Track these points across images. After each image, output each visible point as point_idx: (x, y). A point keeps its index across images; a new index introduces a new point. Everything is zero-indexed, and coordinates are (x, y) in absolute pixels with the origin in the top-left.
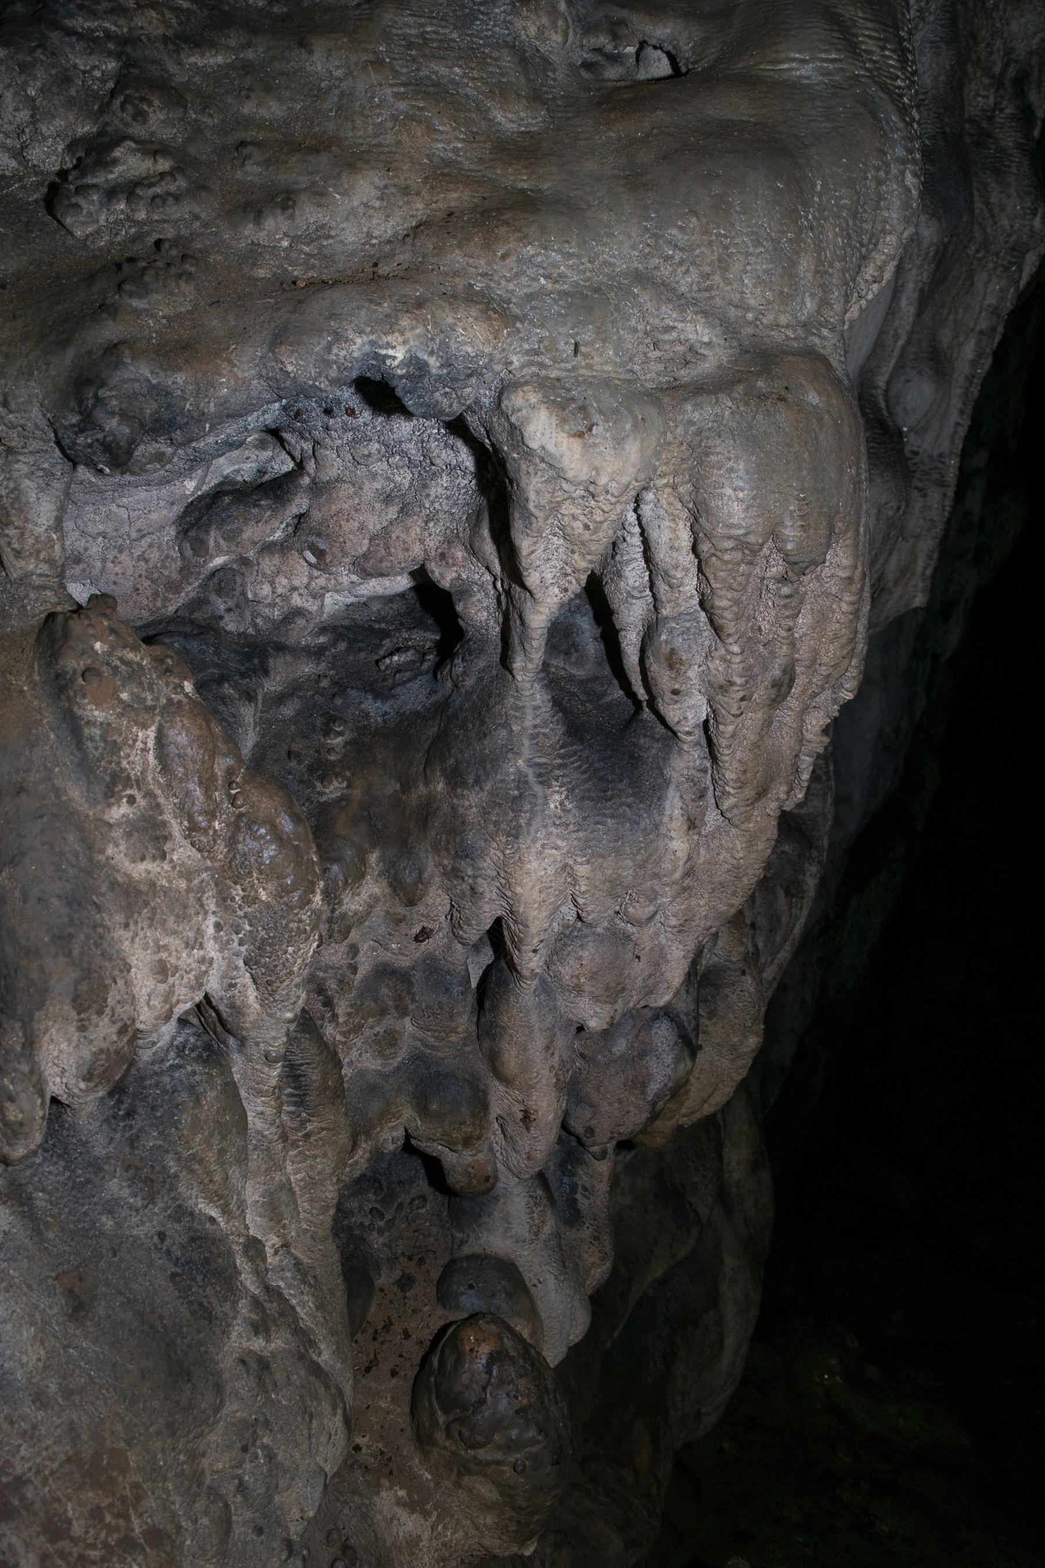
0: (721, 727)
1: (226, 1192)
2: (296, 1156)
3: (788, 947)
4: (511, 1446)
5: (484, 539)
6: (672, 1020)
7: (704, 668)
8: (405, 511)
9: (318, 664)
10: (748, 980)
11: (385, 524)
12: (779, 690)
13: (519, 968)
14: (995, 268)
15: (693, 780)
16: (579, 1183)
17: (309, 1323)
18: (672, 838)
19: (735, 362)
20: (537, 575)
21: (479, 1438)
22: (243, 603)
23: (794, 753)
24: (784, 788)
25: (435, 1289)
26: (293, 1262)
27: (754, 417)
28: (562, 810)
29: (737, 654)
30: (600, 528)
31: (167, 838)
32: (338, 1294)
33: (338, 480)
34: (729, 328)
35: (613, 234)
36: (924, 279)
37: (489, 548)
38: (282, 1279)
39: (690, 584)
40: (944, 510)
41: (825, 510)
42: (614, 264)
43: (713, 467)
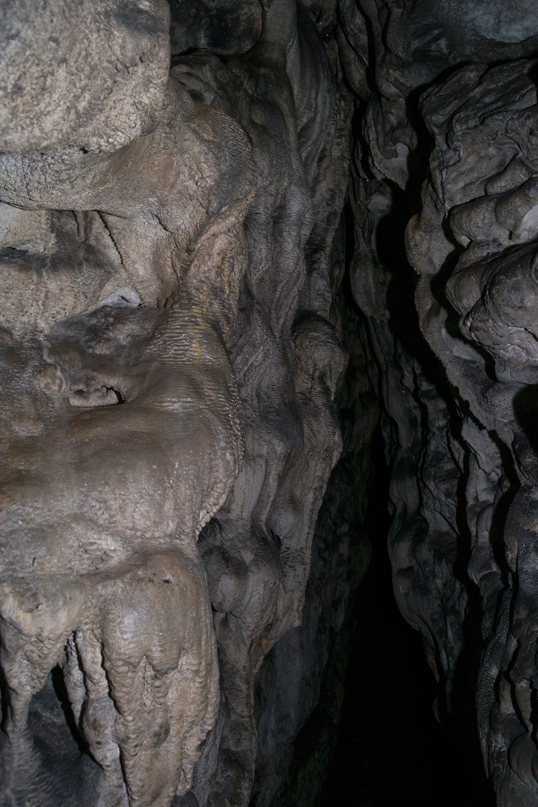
12: (159, 737)
14: (319, 459)
19: (128, 559)
23: (176, 768)
27: (134, 593)
34: (126, 541)
35: (64, 495)
42: (63, 511)
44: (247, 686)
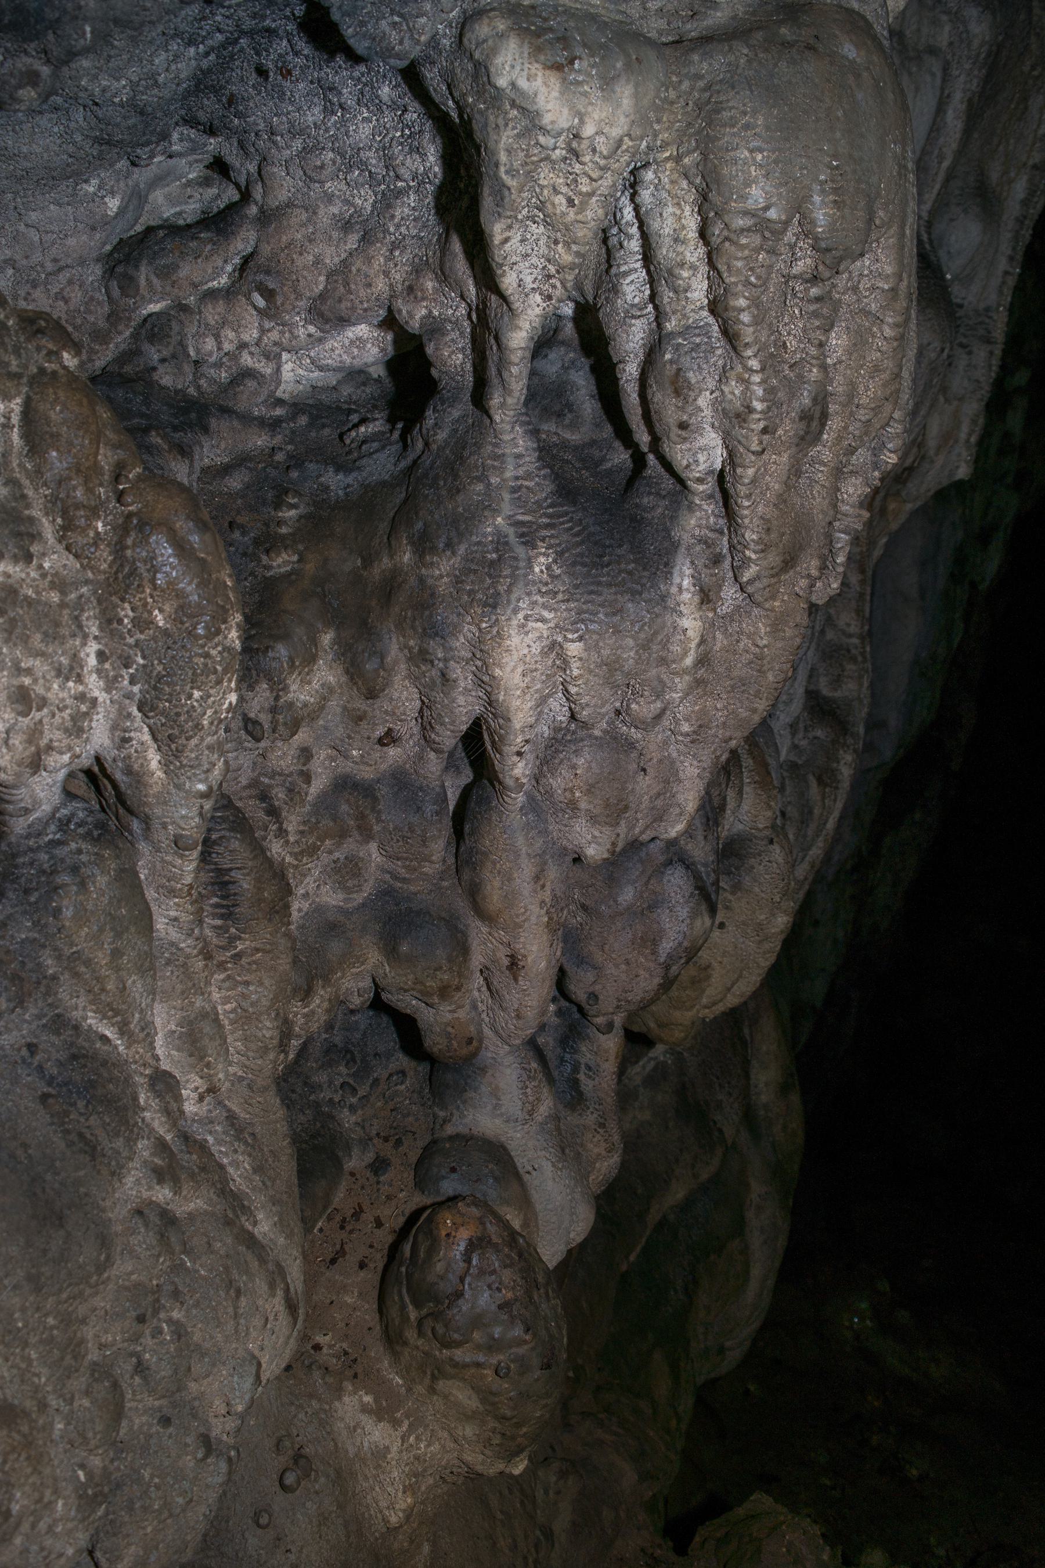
0: (739, 470)
1: (124, 1007)
2: (223, 981)
3: (820, 843)
4: (493, 1346)
5: (456, 255)
6: (687, 867)
7: (717, 394)
8: (366, 239)
9: (272, 437)
10: (776, 848)
11: (344, 256)
12: (808, 426)
13: (501, 776)
15: (706, 543)
16: (582, 1061)
17: (243, 1187)
18: (681, 614)
19: (754, 13)
20: (514, 275)
21: (456, 1336)
22: (179, 356)
24: (815, 563)
25: (412, 1173)
26: (225, 1114)
27: (776, 65)
28: (549, 575)
29: (756, 372)
30: (587, 203)
31: (36, 536)
32: (283, 1159)
33: (290, 204)
36: (973, 88)
37: (460, 266)
38: (210, 1133)
39: (699, 291)
40: (990, 370)
41: (863, 186)
43: (725, 126)
44: (860, 577)
